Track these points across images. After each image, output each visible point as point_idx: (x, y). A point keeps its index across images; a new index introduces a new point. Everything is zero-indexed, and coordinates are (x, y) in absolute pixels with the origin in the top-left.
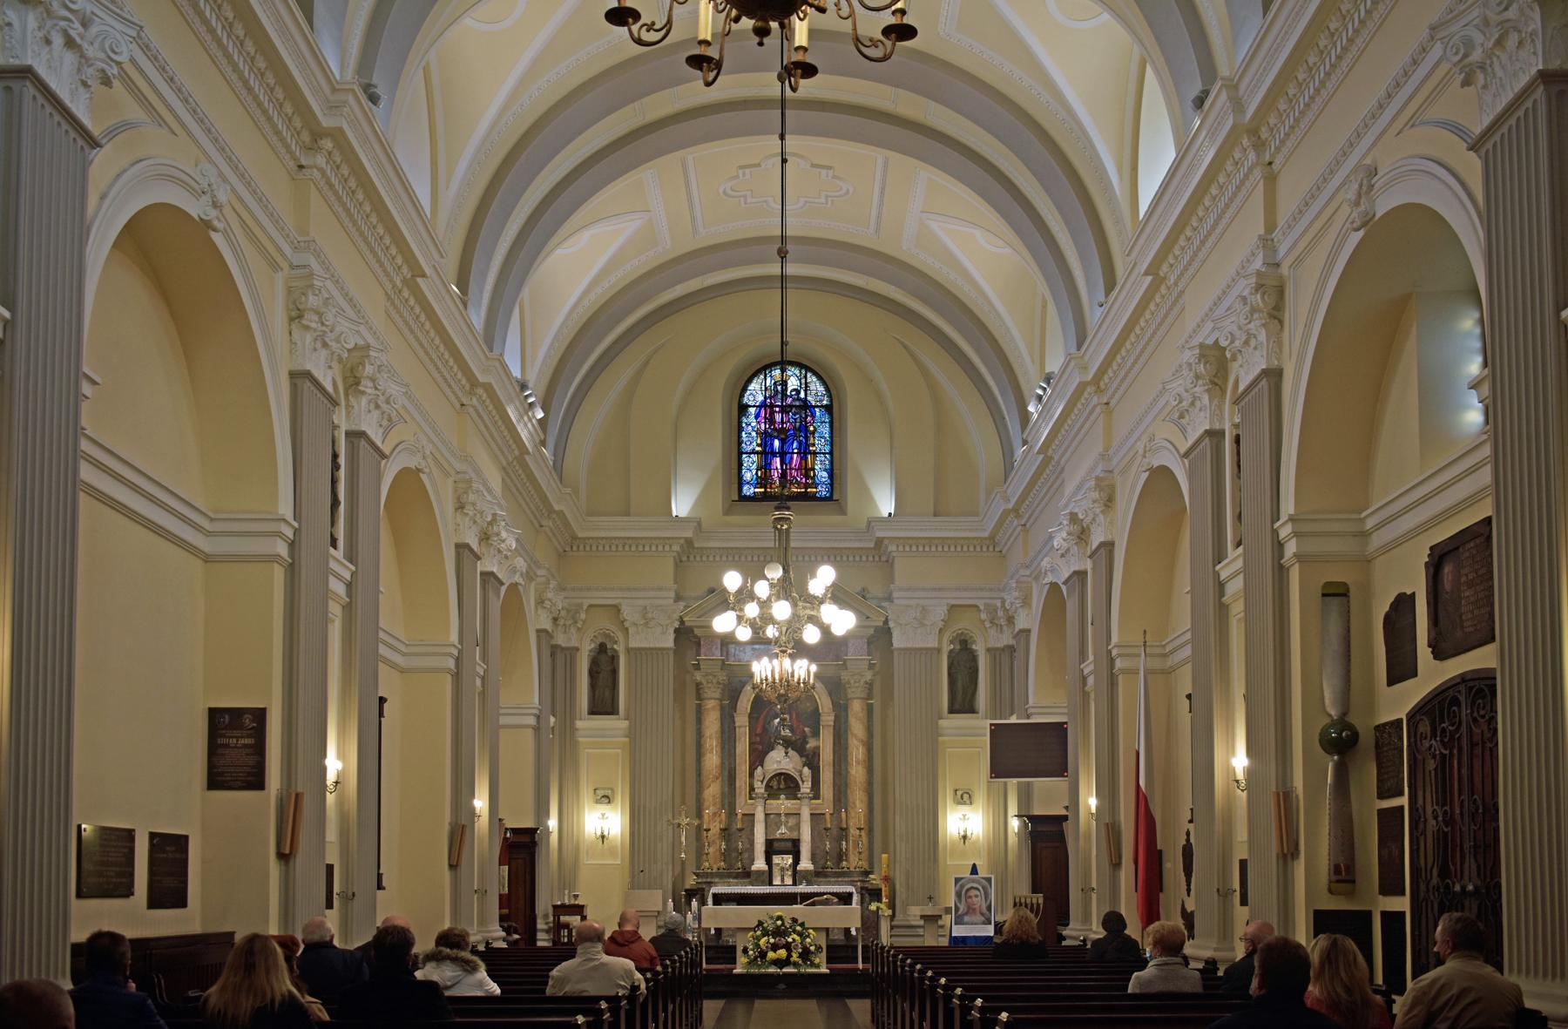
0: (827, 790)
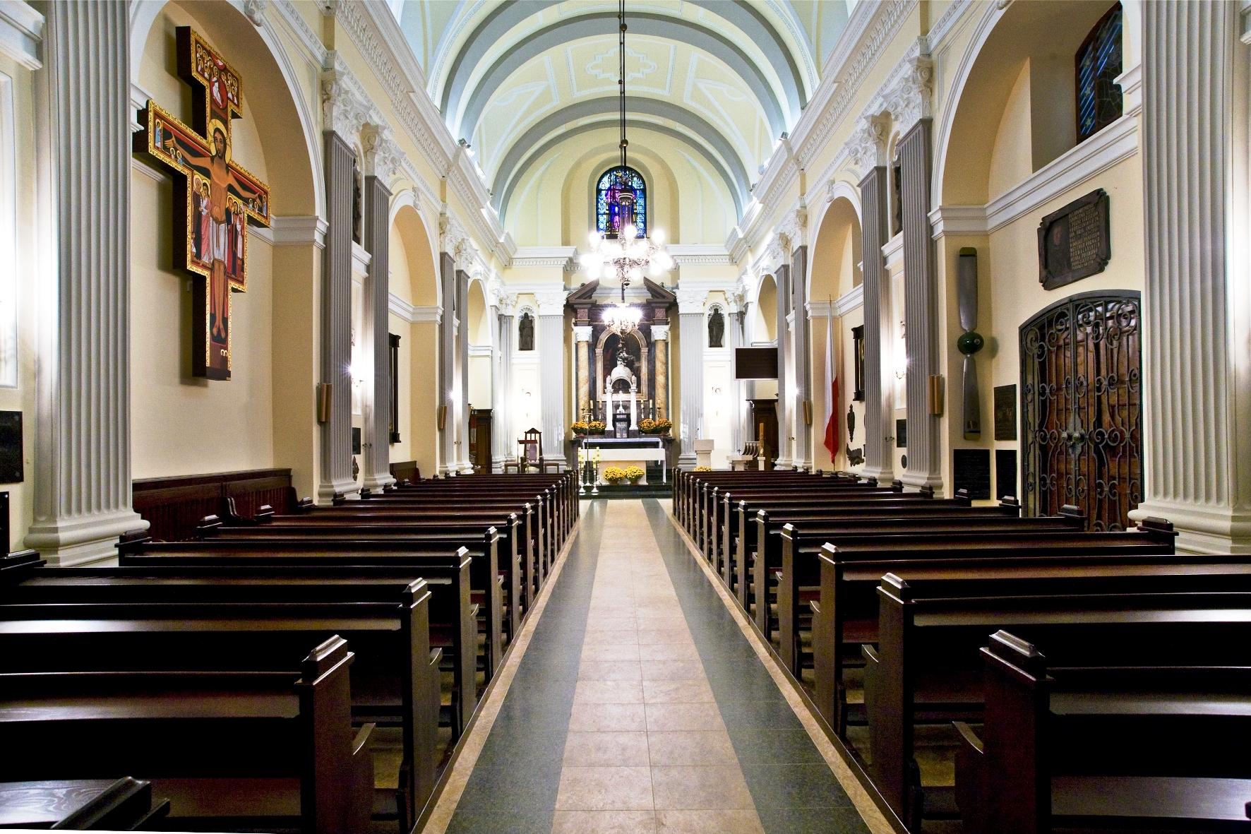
0: (644, 389)
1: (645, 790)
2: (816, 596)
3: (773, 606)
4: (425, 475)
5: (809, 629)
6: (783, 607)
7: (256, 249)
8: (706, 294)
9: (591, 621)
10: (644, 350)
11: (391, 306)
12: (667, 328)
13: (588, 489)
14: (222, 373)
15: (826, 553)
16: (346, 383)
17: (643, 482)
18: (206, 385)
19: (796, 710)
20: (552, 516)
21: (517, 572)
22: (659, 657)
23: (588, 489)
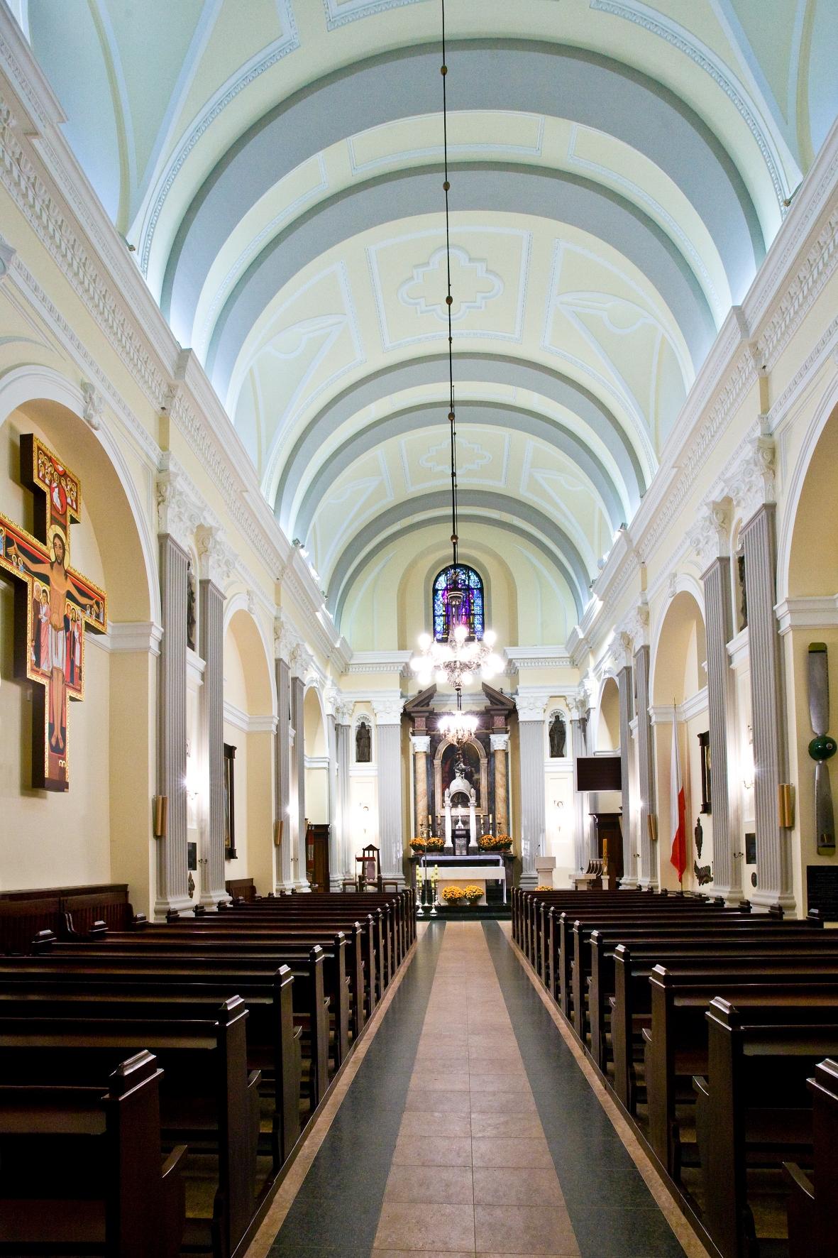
0: (484, 802)
1: (465, 1230)
2: (647, 1023)
3: (608, 1036)
4: (262, 893)
5: (642, 1061)
6: (617, 1037)
7: (93, 653)
8: (546, 700)
9: (422, 1047)
10: (484, 761)
11: (226, 714)
12: (506, 737)
13: (427, 910)
14: (61, 785)
15: (657, 975)
16: (182, 797)
17: (483, 903)
18: (45, 797)
19: (629, 1149)
20: (385, 937)
21: (345, 994)
22: (490, 1088)
23: (427, 910)
